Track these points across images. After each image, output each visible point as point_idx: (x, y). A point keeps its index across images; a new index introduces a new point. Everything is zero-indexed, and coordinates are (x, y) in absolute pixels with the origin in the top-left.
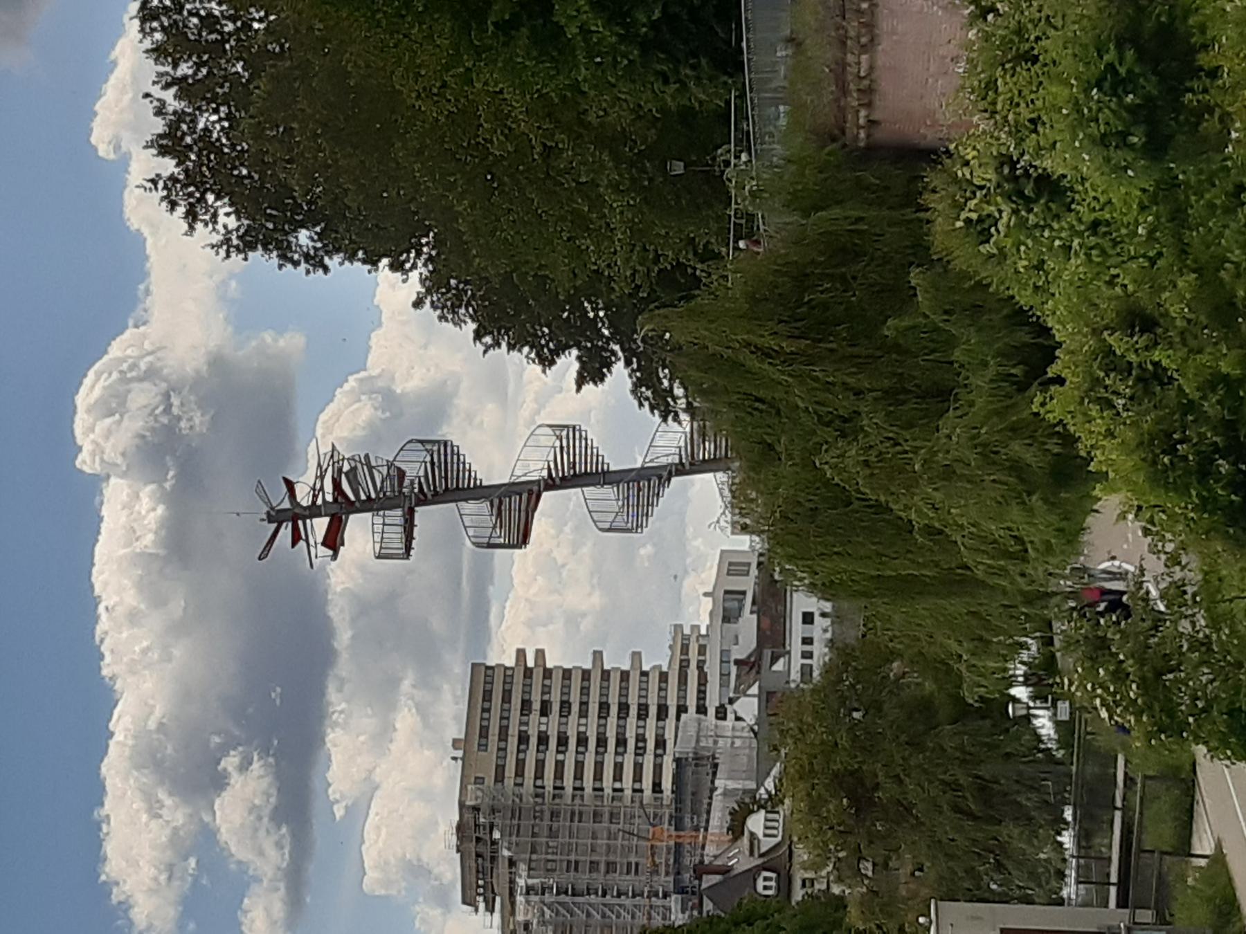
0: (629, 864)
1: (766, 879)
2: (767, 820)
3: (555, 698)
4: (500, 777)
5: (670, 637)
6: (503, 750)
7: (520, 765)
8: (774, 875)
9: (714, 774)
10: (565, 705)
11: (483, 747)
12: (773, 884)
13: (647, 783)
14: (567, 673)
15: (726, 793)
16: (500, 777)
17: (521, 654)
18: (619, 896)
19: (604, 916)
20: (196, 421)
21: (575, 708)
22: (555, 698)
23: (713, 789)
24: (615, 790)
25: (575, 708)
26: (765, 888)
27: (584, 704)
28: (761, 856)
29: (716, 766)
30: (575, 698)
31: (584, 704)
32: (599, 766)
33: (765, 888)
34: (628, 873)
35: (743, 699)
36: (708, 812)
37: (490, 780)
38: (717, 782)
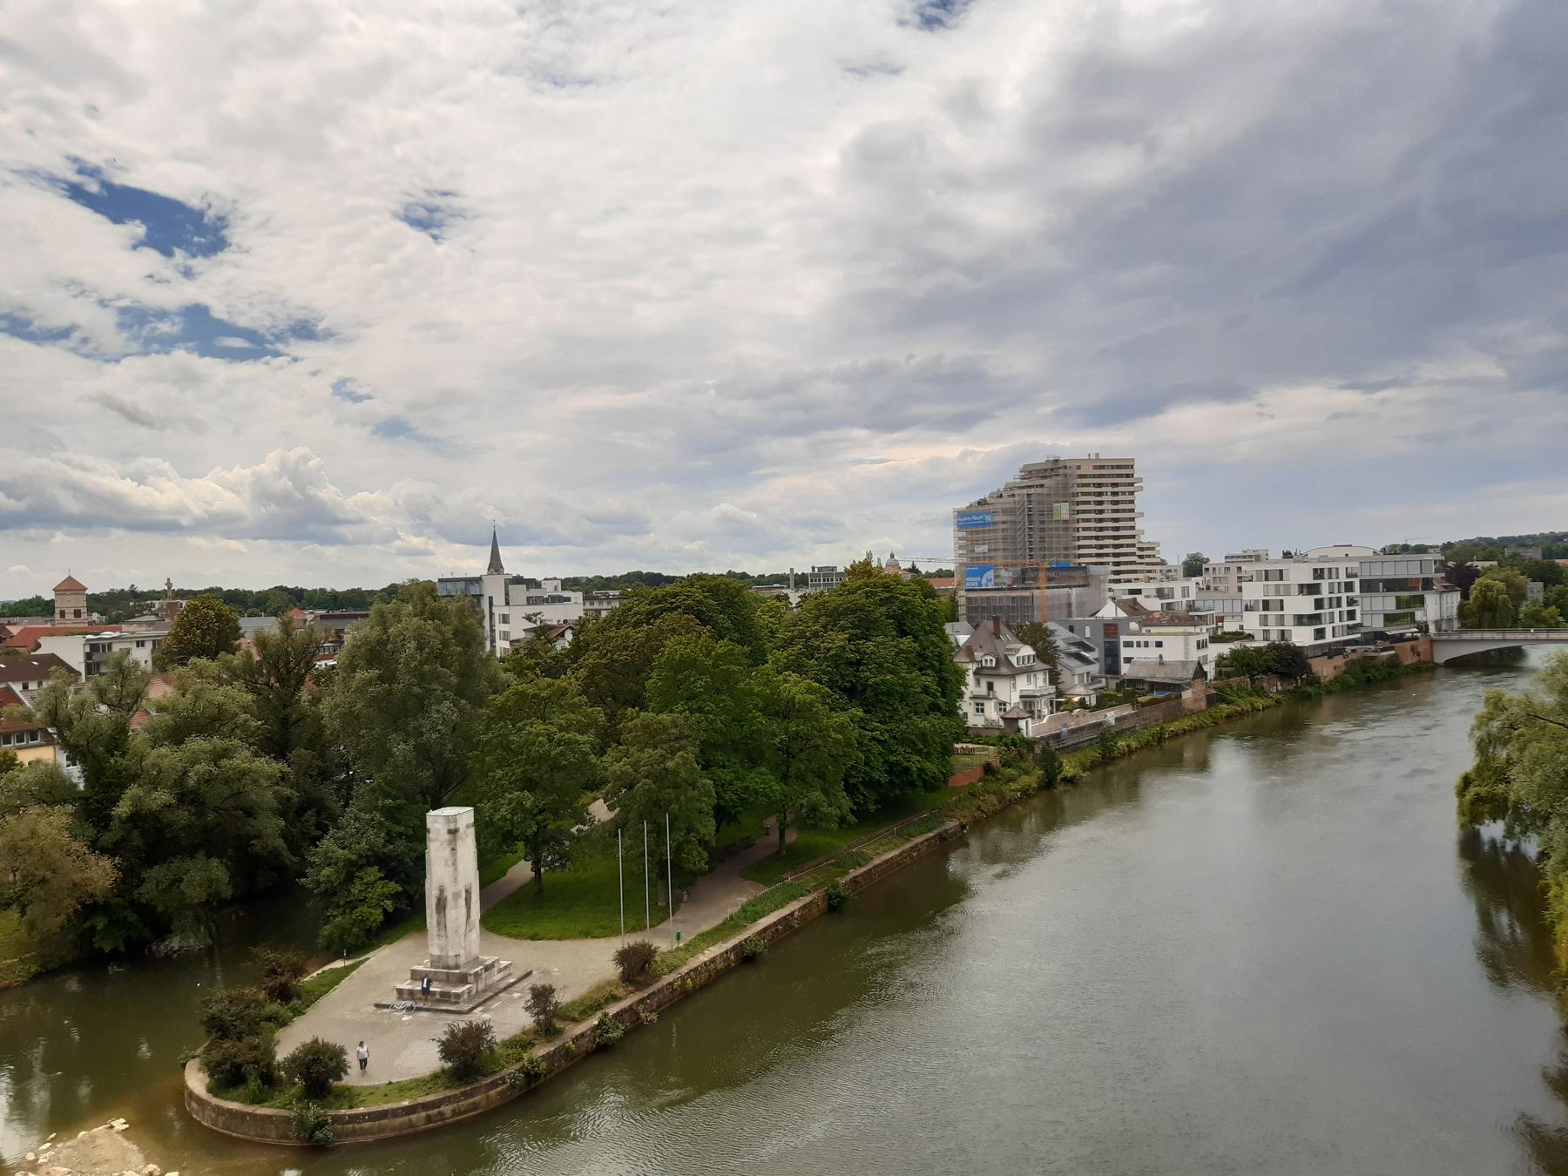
0: (1044, 538)
1: (991, 660)
2: (1029, 657)
3: (1120, 498)
4: (1081, 476)
5: (1154, 541)
6: (1094, 476)
7: (1088, 485)
8: (994, 665)
9: (1079, 586)
10: (1117, 503)
11: (1095, 467)
12: (989, 665)
13: (1083, 542)
14: (1132, 502)
15: (1069, 596)
16: (1081, 476)
17: (1141, 480)
18: (1029, 528)
19: (1020, 529)
20: (67, 783)
21: (1116, 507)
22: (1120, 498)
23: (1070, 587)
24: (1078, 528)
25: (1116, 507)
26: (986, 661)
27: (1117, 511)
28: (1006, 656)
29: (1084, 586)
30: (1120, 507)
31: (1117, 511)
32: (1088, 520)
33: (986, 661)
34: (1041, 538)
35: (1114, 605)
36: (1058, 587)
37: (1079, 472)
38: (1074, 589)
